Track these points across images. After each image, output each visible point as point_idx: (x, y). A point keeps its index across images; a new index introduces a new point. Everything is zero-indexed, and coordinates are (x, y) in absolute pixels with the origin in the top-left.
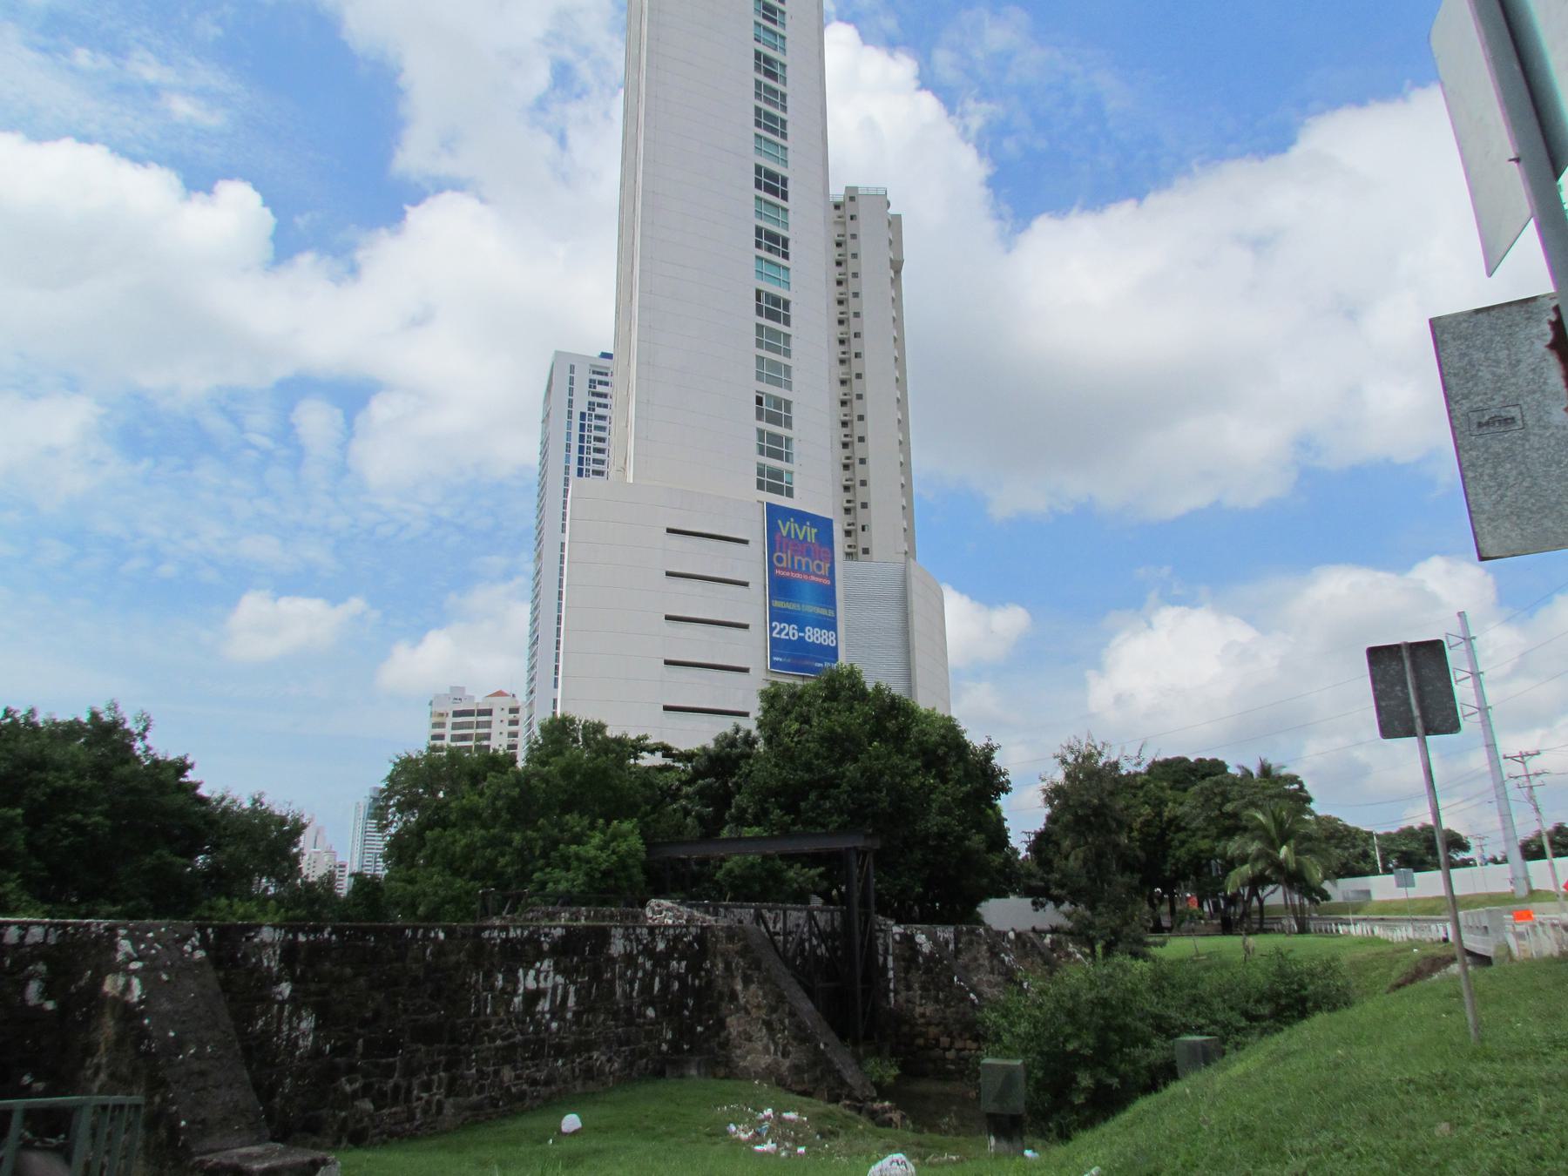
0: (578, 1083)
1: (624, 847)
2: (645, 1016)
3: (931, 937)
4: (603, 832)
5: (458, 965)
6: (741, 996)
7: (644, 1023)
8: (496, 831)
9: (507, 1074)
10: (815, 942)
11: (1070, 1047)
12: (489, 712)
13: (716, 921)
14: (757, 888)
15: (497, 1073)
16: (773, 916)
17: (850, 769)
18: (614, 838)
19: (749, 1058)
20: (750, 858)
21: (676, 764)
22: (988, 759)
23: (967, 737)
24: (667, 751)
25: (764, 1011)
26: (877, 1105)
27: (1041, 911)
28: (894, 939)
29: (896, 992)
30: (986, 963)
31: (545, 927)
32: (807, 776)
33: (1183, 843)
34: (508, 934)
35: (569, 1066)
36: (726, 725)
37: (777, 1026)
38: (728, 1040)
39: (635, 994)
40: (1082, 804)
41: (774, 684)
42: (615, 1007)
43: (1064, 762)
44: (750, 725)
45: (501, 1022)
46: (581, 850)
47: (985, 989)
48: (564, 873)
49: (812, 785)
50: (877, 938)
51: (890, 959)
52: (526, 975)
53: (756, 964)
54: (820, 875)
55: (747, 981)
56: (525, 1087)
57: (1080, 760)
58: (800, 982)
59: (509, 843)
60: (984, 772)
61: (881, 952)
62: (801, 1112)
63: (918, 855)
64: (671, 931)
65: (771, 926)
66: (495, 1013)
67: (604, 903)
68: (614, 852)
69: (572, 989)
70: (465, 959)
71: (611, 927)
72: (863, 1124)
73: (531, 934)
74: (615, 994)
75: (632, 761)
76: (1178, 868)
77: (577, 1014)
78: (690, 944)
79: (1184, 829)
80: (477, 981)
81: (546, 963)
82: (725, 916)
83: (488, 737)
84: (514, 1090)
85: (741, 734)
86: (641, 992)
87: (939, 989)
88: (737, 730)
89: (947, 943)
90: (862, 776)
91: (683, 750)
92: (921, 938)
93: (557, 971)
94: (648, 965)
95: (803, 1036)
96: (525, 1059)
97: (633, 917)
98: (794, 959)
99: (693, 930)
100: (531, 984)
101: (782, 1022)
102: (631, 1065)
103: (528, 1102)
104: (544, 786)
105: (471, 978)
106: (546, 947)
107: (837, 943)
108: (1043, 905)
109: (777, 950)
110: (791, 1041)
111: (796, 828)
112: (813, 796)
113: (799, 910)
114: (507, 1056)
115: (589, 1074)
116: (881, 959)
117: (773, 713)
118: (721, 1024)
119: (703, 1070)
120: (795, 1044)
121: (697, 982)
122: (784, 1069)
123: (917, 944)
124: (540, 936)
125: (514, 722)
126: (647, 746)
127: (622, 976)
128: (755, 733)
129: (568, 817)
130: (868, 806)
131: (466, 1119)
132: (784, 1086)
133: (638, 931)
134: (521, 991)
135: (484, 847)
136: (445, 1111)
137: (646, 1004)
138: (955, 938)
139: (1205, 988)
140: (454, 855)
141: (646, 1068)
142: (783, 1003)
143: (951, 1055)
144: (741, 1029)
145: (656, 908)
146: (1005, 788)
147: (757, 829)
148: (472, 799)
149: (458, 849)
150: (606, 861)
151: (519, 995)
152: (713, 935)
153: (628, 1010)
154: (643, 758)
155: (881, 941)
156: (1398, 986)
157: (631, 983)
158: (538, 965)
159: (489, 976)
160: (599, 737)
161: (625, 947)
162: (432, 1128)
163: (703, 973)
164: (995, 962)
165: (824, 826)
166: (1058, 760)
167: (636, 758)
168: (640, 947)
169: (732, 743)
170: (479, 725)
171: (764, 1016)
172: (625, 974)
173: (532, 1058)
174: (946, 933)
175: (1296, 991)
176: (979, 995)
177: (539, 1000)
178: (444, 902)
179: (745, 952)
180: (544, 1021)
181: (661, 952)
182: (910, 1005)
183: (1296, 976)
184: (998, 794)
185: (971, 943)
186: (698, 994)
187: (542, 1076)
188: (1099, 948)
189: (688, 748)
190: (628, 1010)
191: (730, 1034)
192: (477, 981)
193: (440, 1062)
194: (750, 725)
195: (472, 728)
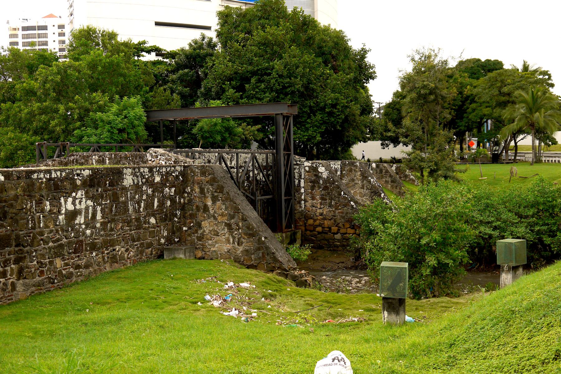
0: (107, 265)
1: (132, 114)
2: (149, 223)
3: (328, 168)
4: (118, 104)
5: (16, 197)
6: (211, 209)
7: (149, 227)
8: (47, 103)
9: (59, 263)
10: (256, 172)
11: (423, 242)
12: (45, 28)
13: (193, 162)
14: (219, 138)
15: (51, 263)
16: (230, 157)
17: (277, 64)
18: (125, 108)
19: (216, 246)
20: (214, 120)
21: (165, 60)
22: (363, 57)
23: (350, 44)
24: (158, 51)
25: (226, 218)
26: (297, 273)
27: (386, 149)
28: (305, 169)
29: (305, 201)
30: (360, 182)
31: (77, 169)
32: (250, 68)
33: (474, 110)
34: (51, 175)
35: (100, 256)
36: (196, 34)
37: (234, 226)
38: (202, 234)
39: (141, 210)
40: (424, 87)
41: (227, 7)
42: (129, 219)
43: (413, 60)
44: (212, 34)
45: (51, 231)
46: (104, 116)
47: (358, 197)
48: (94, 131)
49: (254, 73)
50: (295, 169)
51: (302, 181)
52: (66, 202)
53: (221, 189)
54: (258, 130)
55: (215, 199)
56: (71, 270)
57: (423, 59)
58: (247, 197)
59: (56, 111)
60: (360, 66)
61: (296, 177)
62: (251, 281)
63: (319, 116)
64: (164, 170)
65: (228, 163)
66: (46, 226)
67: (121, 149)
68: (126, 117)
69: (99, 208)
70: (22, 193)
71: (123, 168)
72: (291, 287)
73: (68, 174)
74: (128, 210)
75: (136, 58)
76: (469, 125)
77: (103, 224)
78: (177, 177)
79: (475, 102)
80: (31, 206)
81: (79, 193)
82: (199, 158)
83: (46, 44)
84: (64, 272)
85: (206, 40)
86: (146, 208)
87: (331, 199)
88: (203, 38)
89: (336, 171)
90: (285, 67)
91: (169, 50)
92: (321, 169)
93: (88, 197)
94: (150, 191)
95: (251, 233)
96: (70, 253)
97: (140, 158)
98: (243, 183)
99: (178, 168)
100: (70, 207)
101: (238, 225)
102: (141, 253)
103: (74, 279)
104: (77, 74)
105: (26, 205)
106: (79, 182)
107: (269, 172)
108: (387, 146)
109: (232, 177)
110: (243, 235)
111: (243, 101)
112: (253, 80)
113: (246, 153)
114: (58, 251)
115: (114, 259)
116: (297, 182)
117: (227, 27)
118: (199, 226)
119: (187, 254)
120: (246, 237)
121: (182, 200)
122: (239, 252)
123: (319, 172)
124: (74, 176)
125: (62, 34)
126: (145, 48)
127: (133, 198)
128: (215, 40)
129: (94, 94)
130: (289, 87)
131: (33, 292)
132: (239, 262)
133: (142, 170)
134: (63, 212)
135: (41, 114)
136: (17, 289)
137: (149, 215)
138: (341, 168)
139: (495, 199)
140: (20, 119)
141: (151, 254)
142: (238, 213)
143: (338, 236)
144: (211, 229)
145: (154, 154)
146: (372, 77)
147: (218, 102)
148: (28, 83)
149: (23, 115)
150: (121, 123)
151: (62, 214)
152: (192, 171)
153: (138, 220)
154: (143, 56)
155: (297, 171)
156: (44, 17)
157: (139, 203)
158: (74, 194)
159: (39, 202)
160: (113, 42)
161: (133, 180)
162: (9, 300)
163: (186, 195)
164: (365, 182)
165: (260, 99)
166: (410, 58)
167: (139, 56)
168: (144, 180)
169: (201, 47)
170: (39, 36)
171: (226, 221)
172: (135, 198)
173: (74, 253)
174: (336, 165)
175: (550, 202)
176: (356, 203)
177: (77, 217)
178: (17, 149)
179: (213, 181)
180: (81, 229)
181: (158, 183)
182: (314, 208)
183: (551, 193)
184: (367, 80)
185: (351, 170)
186: (183, 208)
187: (83, 262)
188: (426, 174)
189: (171, 50)
190: (138, 220)
191: (204, 231)
192: (31, 206)
193: (9, 260)
194: (212, 34)
195: (35, 38)
